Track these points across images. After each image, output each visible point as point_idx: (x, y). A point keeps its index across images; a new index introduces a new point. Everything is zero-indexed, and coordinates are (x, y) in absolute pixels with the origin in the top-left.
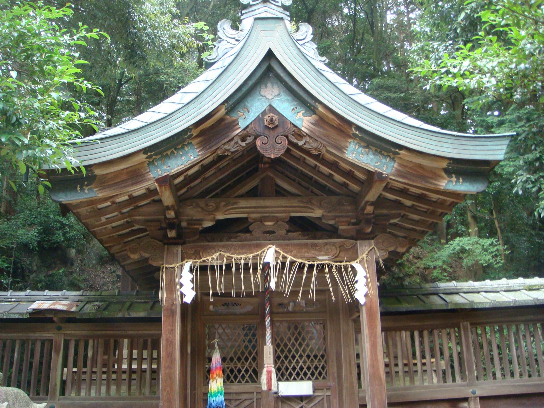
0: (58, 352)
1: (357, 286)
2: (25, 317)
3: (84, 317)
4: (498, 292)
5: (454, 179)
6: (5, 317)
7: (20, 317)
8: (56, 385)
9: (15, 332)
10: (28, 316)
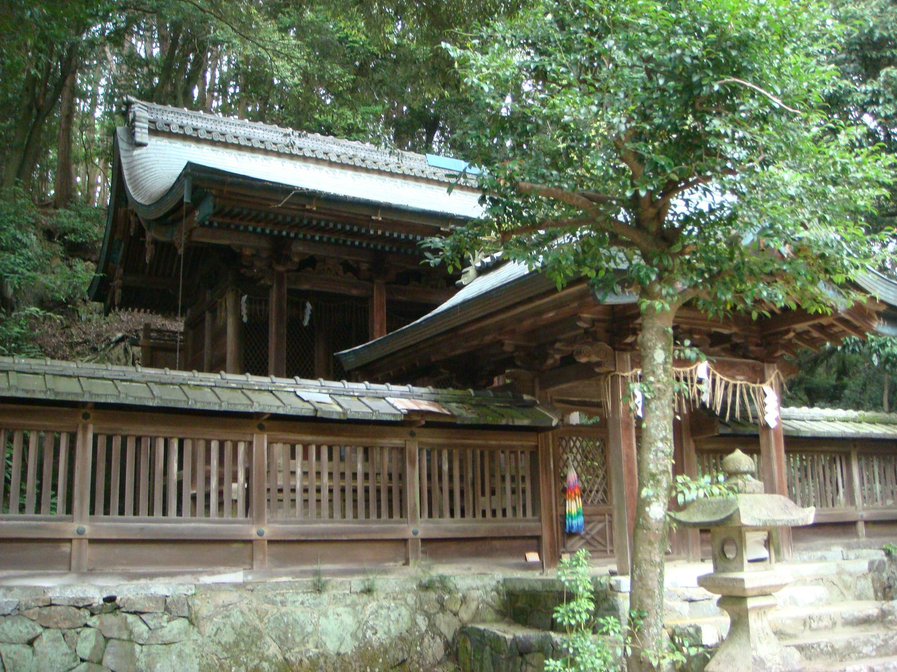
0: (413, 463)
1: (766, 409)
2: (399, 419)
3: (466, 422)
4: (804, 420)
5: (882, 322)
6: (374, 418)
7: (393, 419)
8: (415, 505)
9: (357, 437)
10: (403, 418)
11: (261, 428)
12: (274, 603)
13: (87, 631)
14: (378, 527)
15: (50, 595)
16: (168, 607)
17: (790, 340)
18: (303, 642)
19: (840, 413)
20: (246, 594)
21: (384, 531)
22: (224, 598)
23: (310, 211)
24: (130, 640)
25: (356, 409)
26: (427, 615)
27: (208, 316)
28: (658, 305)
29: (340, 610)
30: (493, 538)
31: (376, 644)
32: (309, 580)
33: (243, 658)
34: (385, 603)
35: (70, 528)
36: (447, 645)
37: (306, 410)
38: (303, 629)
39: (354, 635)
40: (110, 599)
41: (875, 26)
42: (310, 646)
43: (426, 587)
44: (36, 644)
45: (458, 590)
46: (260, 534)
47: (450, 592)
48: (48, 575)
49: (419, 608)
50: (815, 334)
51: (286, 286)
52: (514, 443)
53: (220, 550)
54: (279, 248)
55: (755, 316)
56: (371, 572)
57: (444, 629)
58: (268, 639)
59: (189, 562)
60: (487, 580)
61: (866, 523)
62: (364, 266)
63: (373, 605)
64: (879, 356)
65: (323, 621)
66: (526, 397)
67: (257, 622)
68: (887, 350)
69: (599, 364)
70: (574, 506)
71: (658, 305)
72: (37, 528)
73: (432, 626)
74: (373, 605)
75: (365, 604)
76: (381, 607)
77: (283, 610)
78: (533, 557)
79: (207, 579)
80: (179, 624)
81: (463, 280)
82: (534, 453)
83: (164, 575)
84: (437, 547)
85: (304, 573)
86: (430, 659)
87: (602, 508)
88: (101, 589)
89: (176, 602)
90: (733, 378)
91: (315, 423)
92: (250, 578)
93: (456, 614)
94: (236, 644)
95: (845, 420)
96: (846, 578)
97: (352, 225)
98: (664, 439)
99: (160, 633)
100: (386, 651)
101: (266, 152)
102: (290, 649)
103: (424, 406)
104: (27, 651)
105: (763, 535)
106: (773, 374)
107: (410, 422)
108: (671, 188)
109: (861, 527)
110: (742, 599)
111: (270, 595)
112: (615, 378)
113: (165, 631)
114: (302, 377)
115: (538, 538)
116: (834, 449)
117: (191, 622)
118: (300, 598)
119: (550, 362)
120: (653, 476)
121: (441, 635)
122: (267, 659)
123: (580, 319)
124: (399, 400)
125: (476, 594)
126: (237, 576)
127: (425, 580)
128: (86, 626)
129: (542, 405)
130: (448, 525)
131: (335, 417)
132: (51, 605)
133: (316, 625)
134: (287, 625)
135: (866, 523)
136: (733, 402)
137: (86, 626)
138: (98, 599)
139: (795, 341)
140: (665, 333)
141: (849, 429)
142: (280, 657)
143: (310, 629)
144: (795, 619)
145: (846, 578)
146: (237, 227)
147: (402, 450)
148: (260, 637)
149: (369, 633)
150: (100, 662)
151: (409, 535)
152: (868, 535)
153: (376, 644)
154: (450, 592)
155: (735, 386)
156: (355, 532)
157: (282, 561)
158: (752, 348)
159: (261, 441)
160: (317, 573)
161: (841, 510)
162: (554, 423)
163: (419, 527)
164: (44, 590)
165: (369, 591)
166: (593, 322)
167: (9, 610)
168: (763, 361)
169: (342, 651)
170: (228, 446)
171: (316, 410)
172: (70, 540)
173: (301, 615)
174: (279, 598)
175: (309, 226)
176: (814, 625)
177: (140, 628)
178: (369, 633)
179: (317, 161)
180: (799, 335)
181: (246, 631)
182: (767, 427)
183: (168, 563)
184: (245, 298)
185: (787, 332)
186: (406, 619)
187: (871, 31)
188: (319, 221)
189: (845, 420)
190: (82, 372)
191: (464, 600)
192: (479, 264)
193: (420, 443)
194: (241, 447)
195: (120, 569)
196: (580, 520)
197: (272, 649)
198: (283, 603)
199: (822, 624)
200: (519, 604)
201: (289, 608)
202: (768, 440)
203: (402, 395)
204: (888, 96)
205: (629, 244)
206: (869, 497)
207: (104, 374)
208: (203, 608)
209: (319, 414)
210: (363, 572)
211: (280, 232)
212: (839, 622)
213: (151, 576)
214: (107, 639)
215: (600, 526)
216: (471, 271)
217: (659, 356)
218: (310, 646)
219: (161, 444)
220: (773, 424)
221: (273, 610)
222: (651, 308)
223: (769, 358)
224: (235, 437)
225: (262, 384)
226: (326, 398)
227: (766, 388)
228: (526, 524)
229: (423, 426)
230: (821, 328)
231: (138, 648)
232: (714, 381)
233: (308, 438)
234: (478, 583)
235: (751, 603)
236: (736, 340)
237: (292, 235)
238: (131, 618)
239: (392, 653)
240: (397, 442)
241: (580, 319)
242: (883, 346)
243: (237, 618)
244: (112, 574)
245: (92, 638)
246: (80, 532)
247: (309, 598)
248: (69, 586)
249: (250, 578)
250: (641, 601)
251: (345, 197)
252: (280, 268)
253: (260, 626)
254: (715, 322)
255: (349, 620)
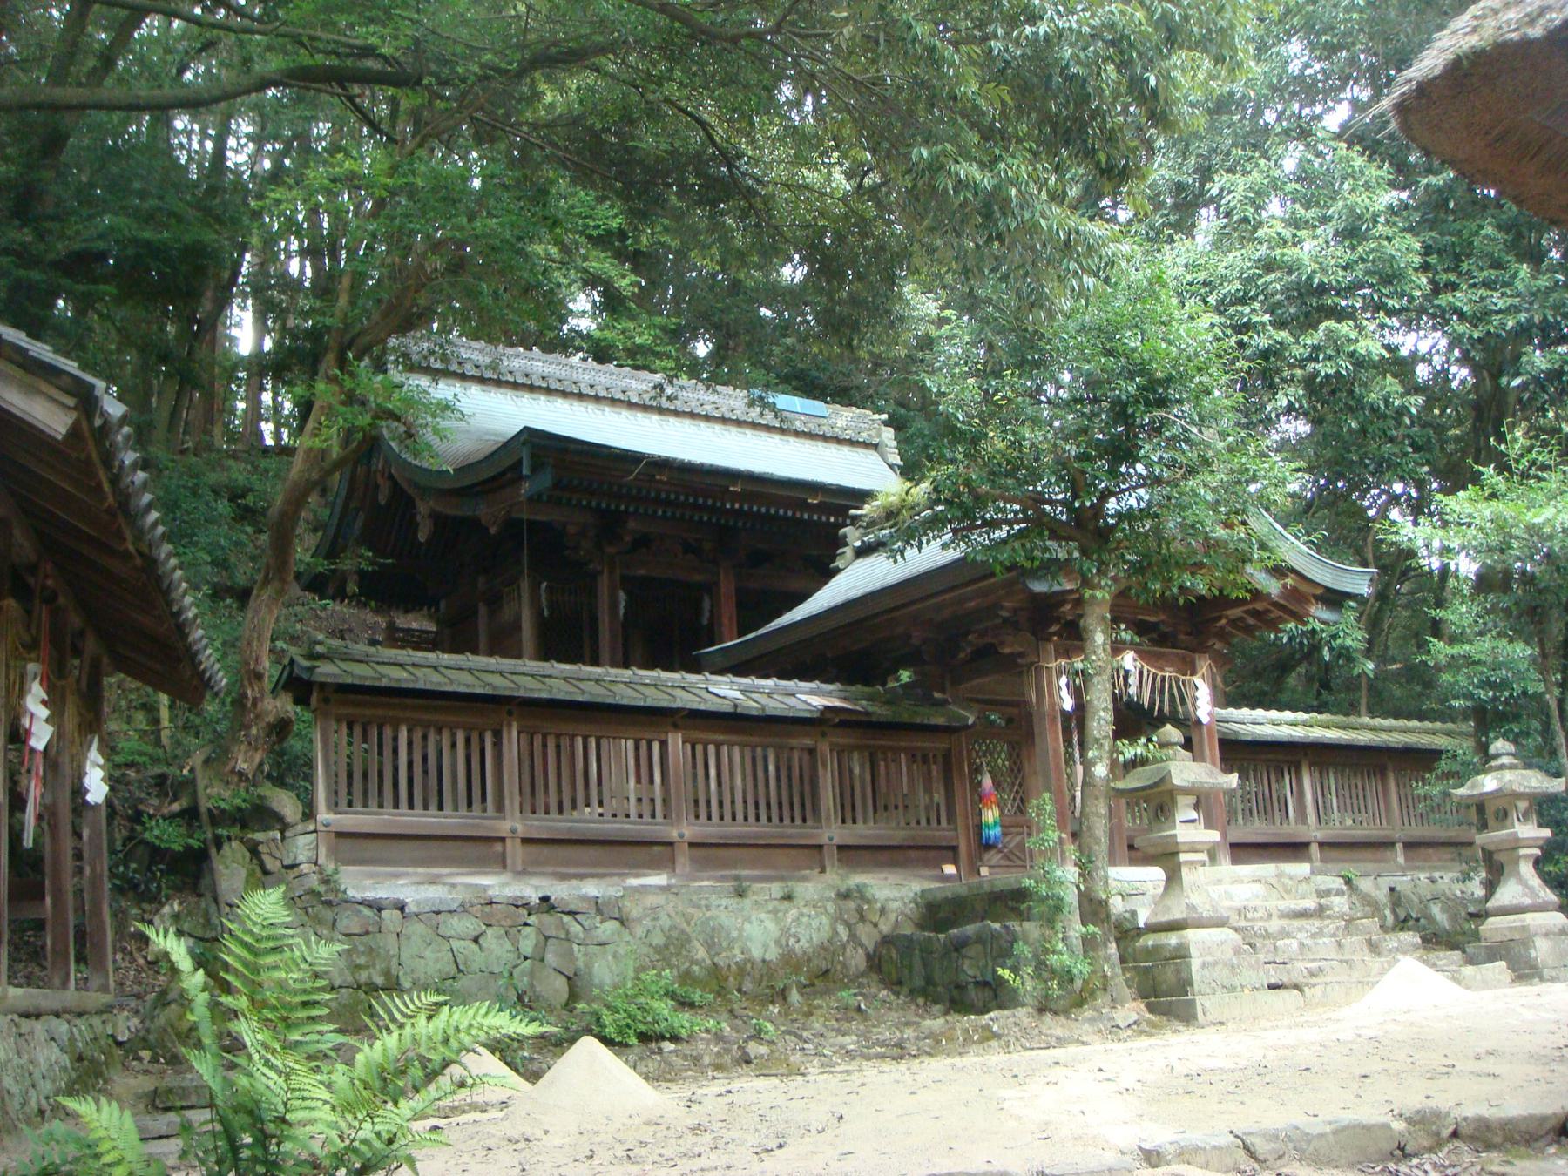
0: (824, 765)
11: (676, 727)
12: (699, 907)
13: (528, 929)
14: (794, 832)
15: (490, 892)
16: (598, 907)
17: (1222, 628)
18: (730, 948)
19: (1288, 715)
20: (671, 897)
21: (801, 836)
22: (652, 900)
23: (661, 482)
24: (568, 940)
25: (775, 706)
26: (848, 925)
27: (483, 610)
28: (1099, 594)
29: (763, 916)
30: (910, 847)
31: (799, 952)
32: (729, 885)
33: (674, 961)
34: (805, 911)
35: (504, 827)
36: (869, 957)
37: (726, 707)
38: (728, 934)
39: (777, 942)
40: (545, 899)
41: (1314, 272)
42: (737, 951)
43: (845, 896)
44: (481, 941)
45: (876, 901)
46: (681, 836)
47: (868, 902)
48: (486, 873)
49: (838, 918)
50: (1251, 621)
51: (618, 572)
52: (926, 744)
53: (640, 853)
54: (609, 525)
55: (1181, 601)
56: (791, 878)
57: (864, 939)
58: (696, 943)
59: (615, 865)
60: (904, 891)
61: (1321, 845)
62: (707, 546)
63: (793, 913)
64: (1331, 649)
65: (747, 926)
66: (936, 695)
67: (685, 925)
68: (1339, 641)
69: (1021, 655)
70: (990, 815)
71: (1099, 594)
72: (473, 826)
73: (853, 936)
74: (793, 913)
75: (787, 911)
76: (802, 915)
77: (708, 914)
78: (950, 869)
79: (633, 882)
80: (610, 926)
81: (839, 563)
82: (947, 757)
83: (593, 876)
84: (852, 854)
85: (723, 879)
86: (853, 970)
87: (1020, 818)
88: (537, 888)
89: (608, 902)
90: (1162, 670)
91: (733, 722)
92: (673, 881)
93: (876, 925)
94: (666, 946)
95: (1293, 724)
96: (1287, 881)
97: (706, 498)
98: (1105, 709)
99: (594, 933)
100: (809, 960)
101: (548, 391)
102: (718, 954)
103: (837, 703)
104: (474, 946)
105: (1192, 799)
106: (1204, 665)
107: (822, 721)
108: (1105, 495)
109: (1314, 848)
110: (1176, 853)
111: (695, 898)
112: (1039, 669)
113: (599, 931)
114: (712, 673)
115: (954, 849)
116: (1280, 757)
117: (622, 923)
118: (724, 902)
119: (962, 655)
120: (1097, 740)
121: (862, 946)
122: (696, 963)
123: (1002, 607)
124: (811, 697)
125: (894, 905)
126: (659, 879)
127: (843, 890)
128: (526, 924)
129: (954, 702)
130: (864, 831)
131: (754, 713)
132: (491, 903)
133: (741, 930)
134: (713, 929)
135: (1321, 845)
136: (1162, 701)
137: (526, 924)
138: (534, 897)
139: (1228, 629)
140: (1104, 618)
141: (1298, 733)
142: (709, 962)
143: (735, 934)
144: (1230, 908)
145: (1287, 881)
146: (569, 500)
147: (812, 752)
148: (689, 940)
149: (792, 941)
150: (542, 960)
151: (824, 840)
152: (1323, 861)
153: (799, 952)
154: (868, 902)
155: (1163, 679)
156: (772, 836)
157: (702, 865)
158: (1182, 637)
159: (676, 741)
160: (737, 878)
161: (1291, 830)
162: (970, 722)
163: (833, 832)
164: (485, 888)
165: (788, 897)
166: (1015, 611)
167: (454, 906)
168: (1194, 651)
169: (767, 957)
170: (644, 744)
171: (736, 706)
172: (503, 839)
173: (725, 919)
174: (703, 902)
175: (657, 501)
176: (1249, 916)
177: (575, 928)
178: (792, 941)
179: (613, 401)
180: (1233, 622)
181: (675, 934)
182: (1199, 722)
183: (594, 864)
184: (544, 585)
185: (1220, 618)
186: (827, 928)
187: (1310, 278)
188: (668, 493)
189: (1293, 724)
190: (504, 668)
191: (883, 911)
192: (858, 544)
193: (831, 744)
194: (656, 746)
195: (550, 869)
196: (997, 831)
197: (701, 953)
198: (708, 907)
199: (1257, 915)
200: (941, 915)
201: (713, 912)
202: (1201, 735)
203: (812, 692)
204: (1329, 352)
205: (1068, 539)
206: (1322, 811)
207: (525, 669)
208: (633, 909)
209: (739, 710)
210: (782, 879)
211: (618, 506)
212: (1275, 913)
213: (582, 877)
214: (547, 938)
215: (1018, 839)
216: (848, 551)
217: (1099, 638)
218: (737, 951)
219: (579, 740)
220: (1205, 719)
221: (698, 914)
222: (1093, 597)
223: (1201, 648)
224: (649, 736)
225: (674, 680)
226: (738, 694)
227: (1197, 680)
228: (941, 833)
229: (836, 726)
230: (1257, 614)
231: (576, 947)
232: (1141, 673)
233: (722, 737)
234: (895, 893)
235: (1183, 857)
236: (1164, 628)
237: (631, 509)
238: (566, 918)
239: (816, 962)
240: (808, 742)
241: (1002, 607)
242: (1335, 637)
243: (665, 921)
244: (543, 874)
245: (533, 936)
246: (513, 831)
247: (732, 902)
248: (507, 884)
249: (673, 881)
250: (1090, 848)
251: (702, 465)
252: (611, 550)
253: (688, 930)
254: (1146, 609)
255: (771, 926)
